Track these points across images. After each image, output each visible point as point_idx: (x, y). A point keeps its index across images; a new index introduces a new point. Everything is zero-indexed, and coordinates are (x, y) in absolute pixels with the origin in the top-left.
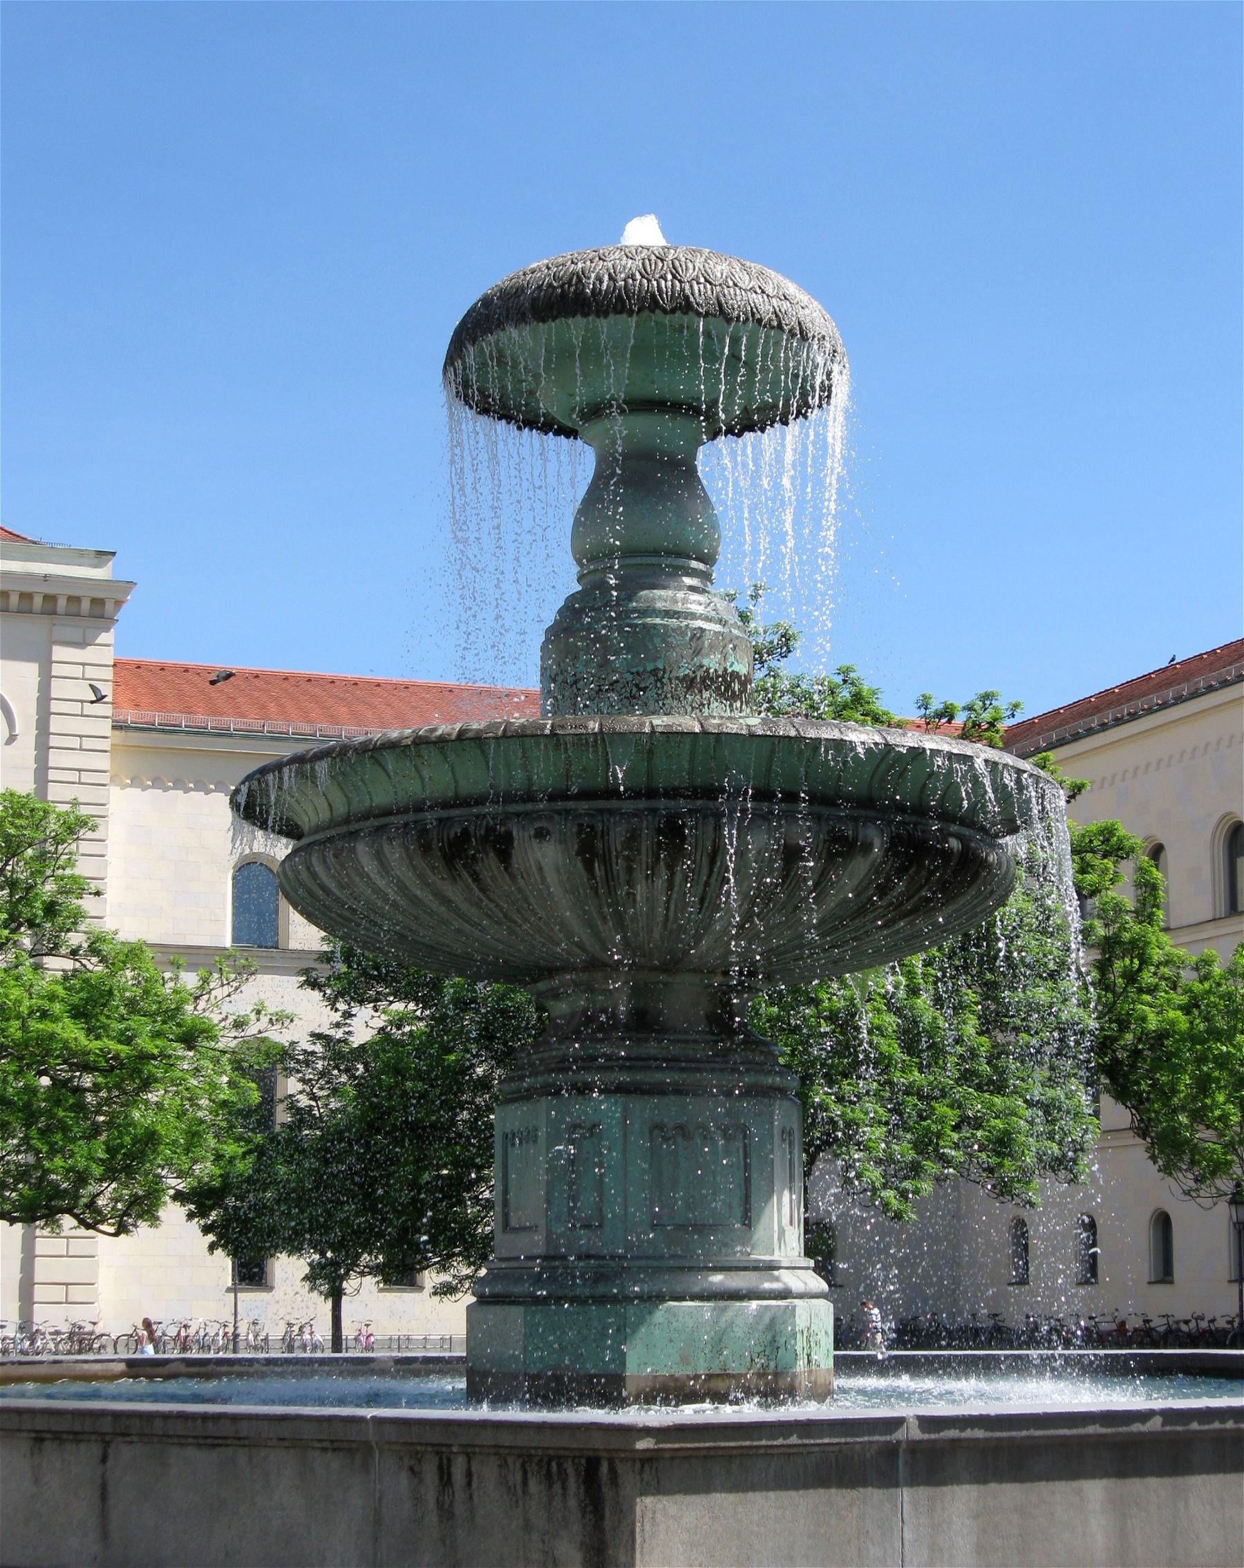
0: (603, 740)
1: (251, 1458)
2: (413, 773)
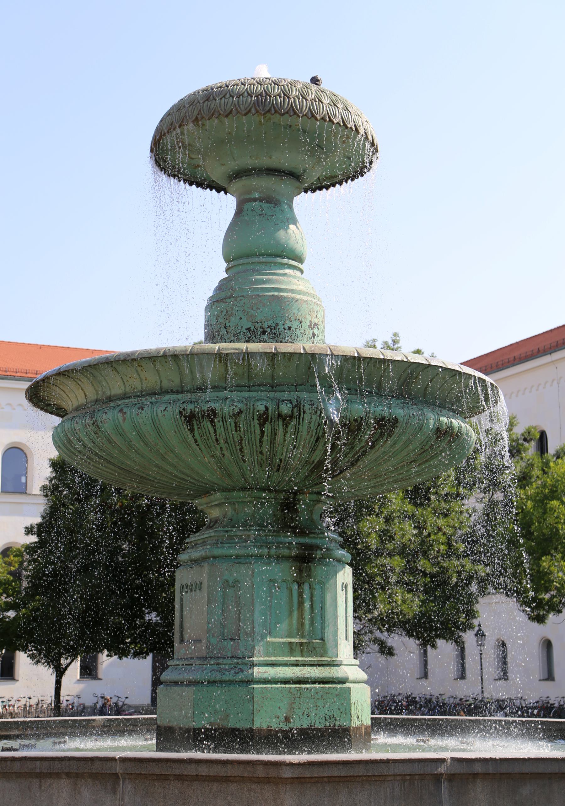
0: (248, 356)
1: (40, 786)
2: (136, 376)
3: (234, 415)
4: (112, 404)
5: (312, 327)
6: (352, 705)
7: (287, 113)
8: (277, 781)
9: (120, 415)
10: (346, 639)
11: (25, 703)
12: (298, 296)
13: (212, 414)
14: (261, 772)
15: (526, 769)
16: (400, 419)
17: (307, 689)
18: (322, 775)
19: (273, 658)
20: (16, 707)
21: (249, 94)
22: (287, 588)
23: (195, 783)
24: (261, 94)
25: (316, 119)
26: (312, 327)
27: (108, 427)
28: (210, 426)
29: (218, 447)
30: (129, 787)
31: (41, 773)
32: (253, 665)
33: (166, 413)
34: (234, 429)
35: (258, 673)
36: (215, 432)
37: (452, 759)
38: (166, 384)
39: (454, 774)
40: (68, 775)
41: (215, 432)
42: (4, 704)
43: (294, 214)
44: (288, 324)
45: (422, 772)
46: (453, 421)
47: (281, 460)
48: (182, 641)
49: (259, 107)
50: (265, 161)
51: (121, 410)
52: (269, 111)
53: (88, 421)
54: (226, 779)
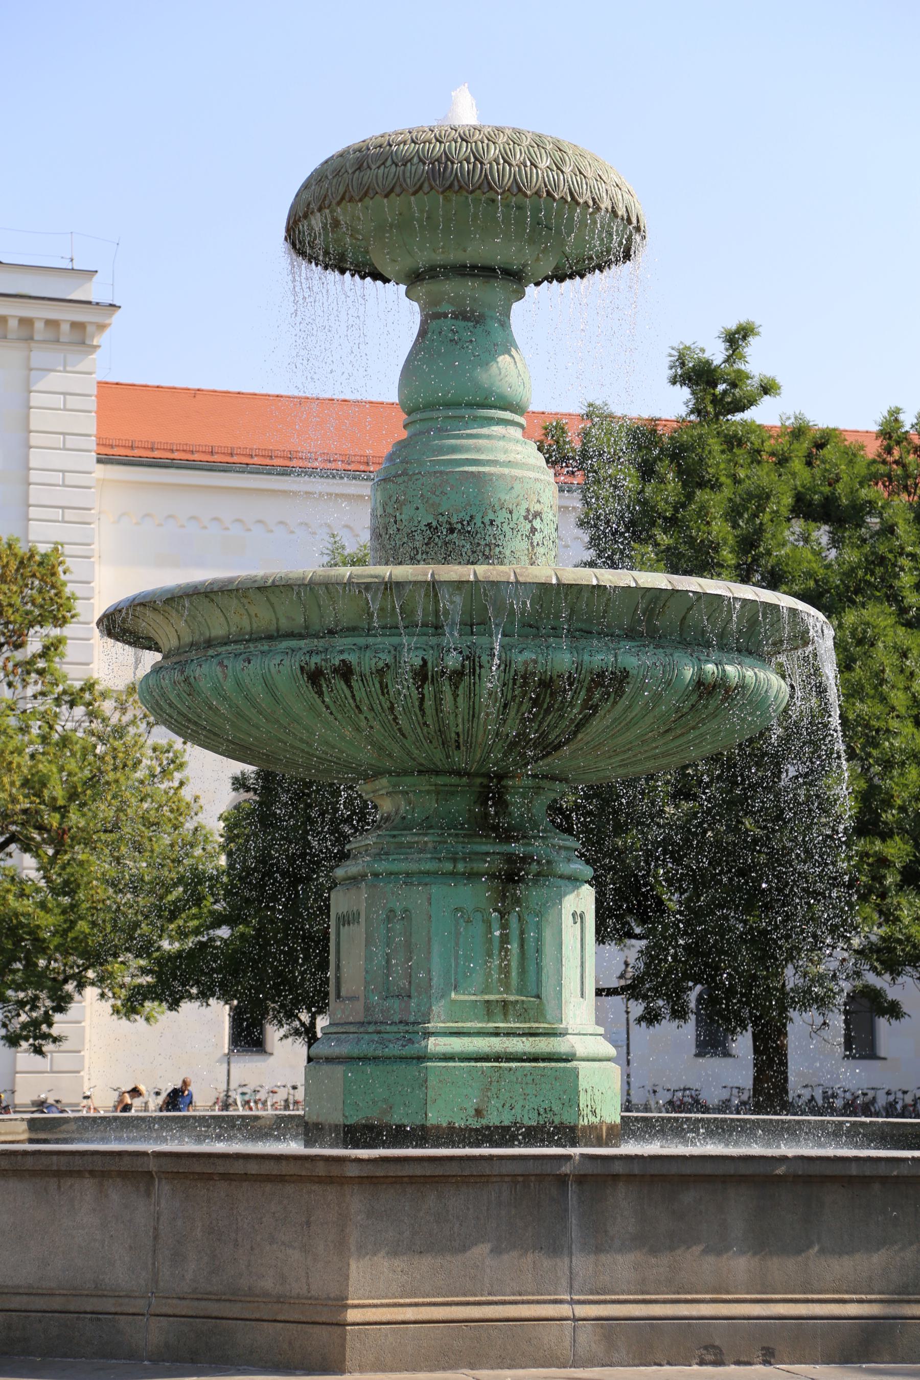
1: (59, 1187)
3: (378, 671)
4: (211, 652)
5: (530, 517)
6: (582, 1094)
7: (479, 188)
8: (341, 1181)
9: (219, 669)
10: (582, 996)
11: (285, 1097)
12: (506, 471)
13: (345, 672)
14: (321, 1170)
15: (687, 1170)
16: (633, 672)
17: (510, 1069)
18: (400, 1174)
19: (460, 1025)
20: (269, 1103)
21: (421, 160)
22: (483, 921)
23: (245, 1184)
24: (438, 160)
25: (525, 195)
26: (530, 517)
27: (205, 685)
28: (345, 687)
29: (362, 717)
30: (166, 1188)
31: (58, 1171)
32: (428, 1034)
33: (281, 668)
34: (379, 692)
35: (435, 1045)
36: (353, 696)
37: (582, 1155)
38: (284, 624)
39: (585, 1175)
40: (92, 1173)
41: (353, 696)
42: (247, 1098)
43: (510, 334)
44: (491, 516)
45: (538, 1172)
46: (729, 669)
47: (458, 734)
48: (338, 996)
49: (435, 181)
50: (454, 256)
51: (221, 664)
52: (451, 186)
53: (177, 677)
54: (281, 1179)
